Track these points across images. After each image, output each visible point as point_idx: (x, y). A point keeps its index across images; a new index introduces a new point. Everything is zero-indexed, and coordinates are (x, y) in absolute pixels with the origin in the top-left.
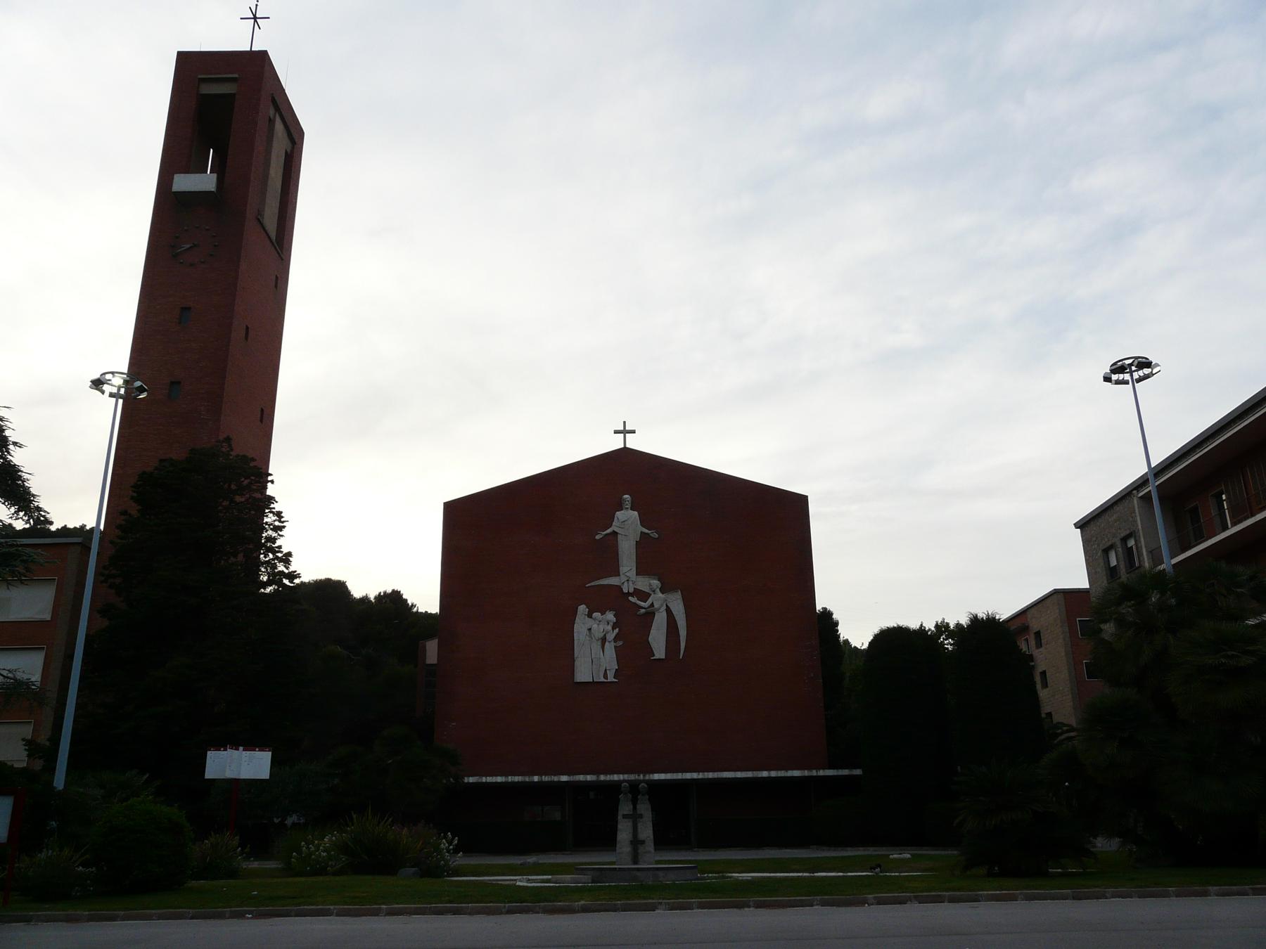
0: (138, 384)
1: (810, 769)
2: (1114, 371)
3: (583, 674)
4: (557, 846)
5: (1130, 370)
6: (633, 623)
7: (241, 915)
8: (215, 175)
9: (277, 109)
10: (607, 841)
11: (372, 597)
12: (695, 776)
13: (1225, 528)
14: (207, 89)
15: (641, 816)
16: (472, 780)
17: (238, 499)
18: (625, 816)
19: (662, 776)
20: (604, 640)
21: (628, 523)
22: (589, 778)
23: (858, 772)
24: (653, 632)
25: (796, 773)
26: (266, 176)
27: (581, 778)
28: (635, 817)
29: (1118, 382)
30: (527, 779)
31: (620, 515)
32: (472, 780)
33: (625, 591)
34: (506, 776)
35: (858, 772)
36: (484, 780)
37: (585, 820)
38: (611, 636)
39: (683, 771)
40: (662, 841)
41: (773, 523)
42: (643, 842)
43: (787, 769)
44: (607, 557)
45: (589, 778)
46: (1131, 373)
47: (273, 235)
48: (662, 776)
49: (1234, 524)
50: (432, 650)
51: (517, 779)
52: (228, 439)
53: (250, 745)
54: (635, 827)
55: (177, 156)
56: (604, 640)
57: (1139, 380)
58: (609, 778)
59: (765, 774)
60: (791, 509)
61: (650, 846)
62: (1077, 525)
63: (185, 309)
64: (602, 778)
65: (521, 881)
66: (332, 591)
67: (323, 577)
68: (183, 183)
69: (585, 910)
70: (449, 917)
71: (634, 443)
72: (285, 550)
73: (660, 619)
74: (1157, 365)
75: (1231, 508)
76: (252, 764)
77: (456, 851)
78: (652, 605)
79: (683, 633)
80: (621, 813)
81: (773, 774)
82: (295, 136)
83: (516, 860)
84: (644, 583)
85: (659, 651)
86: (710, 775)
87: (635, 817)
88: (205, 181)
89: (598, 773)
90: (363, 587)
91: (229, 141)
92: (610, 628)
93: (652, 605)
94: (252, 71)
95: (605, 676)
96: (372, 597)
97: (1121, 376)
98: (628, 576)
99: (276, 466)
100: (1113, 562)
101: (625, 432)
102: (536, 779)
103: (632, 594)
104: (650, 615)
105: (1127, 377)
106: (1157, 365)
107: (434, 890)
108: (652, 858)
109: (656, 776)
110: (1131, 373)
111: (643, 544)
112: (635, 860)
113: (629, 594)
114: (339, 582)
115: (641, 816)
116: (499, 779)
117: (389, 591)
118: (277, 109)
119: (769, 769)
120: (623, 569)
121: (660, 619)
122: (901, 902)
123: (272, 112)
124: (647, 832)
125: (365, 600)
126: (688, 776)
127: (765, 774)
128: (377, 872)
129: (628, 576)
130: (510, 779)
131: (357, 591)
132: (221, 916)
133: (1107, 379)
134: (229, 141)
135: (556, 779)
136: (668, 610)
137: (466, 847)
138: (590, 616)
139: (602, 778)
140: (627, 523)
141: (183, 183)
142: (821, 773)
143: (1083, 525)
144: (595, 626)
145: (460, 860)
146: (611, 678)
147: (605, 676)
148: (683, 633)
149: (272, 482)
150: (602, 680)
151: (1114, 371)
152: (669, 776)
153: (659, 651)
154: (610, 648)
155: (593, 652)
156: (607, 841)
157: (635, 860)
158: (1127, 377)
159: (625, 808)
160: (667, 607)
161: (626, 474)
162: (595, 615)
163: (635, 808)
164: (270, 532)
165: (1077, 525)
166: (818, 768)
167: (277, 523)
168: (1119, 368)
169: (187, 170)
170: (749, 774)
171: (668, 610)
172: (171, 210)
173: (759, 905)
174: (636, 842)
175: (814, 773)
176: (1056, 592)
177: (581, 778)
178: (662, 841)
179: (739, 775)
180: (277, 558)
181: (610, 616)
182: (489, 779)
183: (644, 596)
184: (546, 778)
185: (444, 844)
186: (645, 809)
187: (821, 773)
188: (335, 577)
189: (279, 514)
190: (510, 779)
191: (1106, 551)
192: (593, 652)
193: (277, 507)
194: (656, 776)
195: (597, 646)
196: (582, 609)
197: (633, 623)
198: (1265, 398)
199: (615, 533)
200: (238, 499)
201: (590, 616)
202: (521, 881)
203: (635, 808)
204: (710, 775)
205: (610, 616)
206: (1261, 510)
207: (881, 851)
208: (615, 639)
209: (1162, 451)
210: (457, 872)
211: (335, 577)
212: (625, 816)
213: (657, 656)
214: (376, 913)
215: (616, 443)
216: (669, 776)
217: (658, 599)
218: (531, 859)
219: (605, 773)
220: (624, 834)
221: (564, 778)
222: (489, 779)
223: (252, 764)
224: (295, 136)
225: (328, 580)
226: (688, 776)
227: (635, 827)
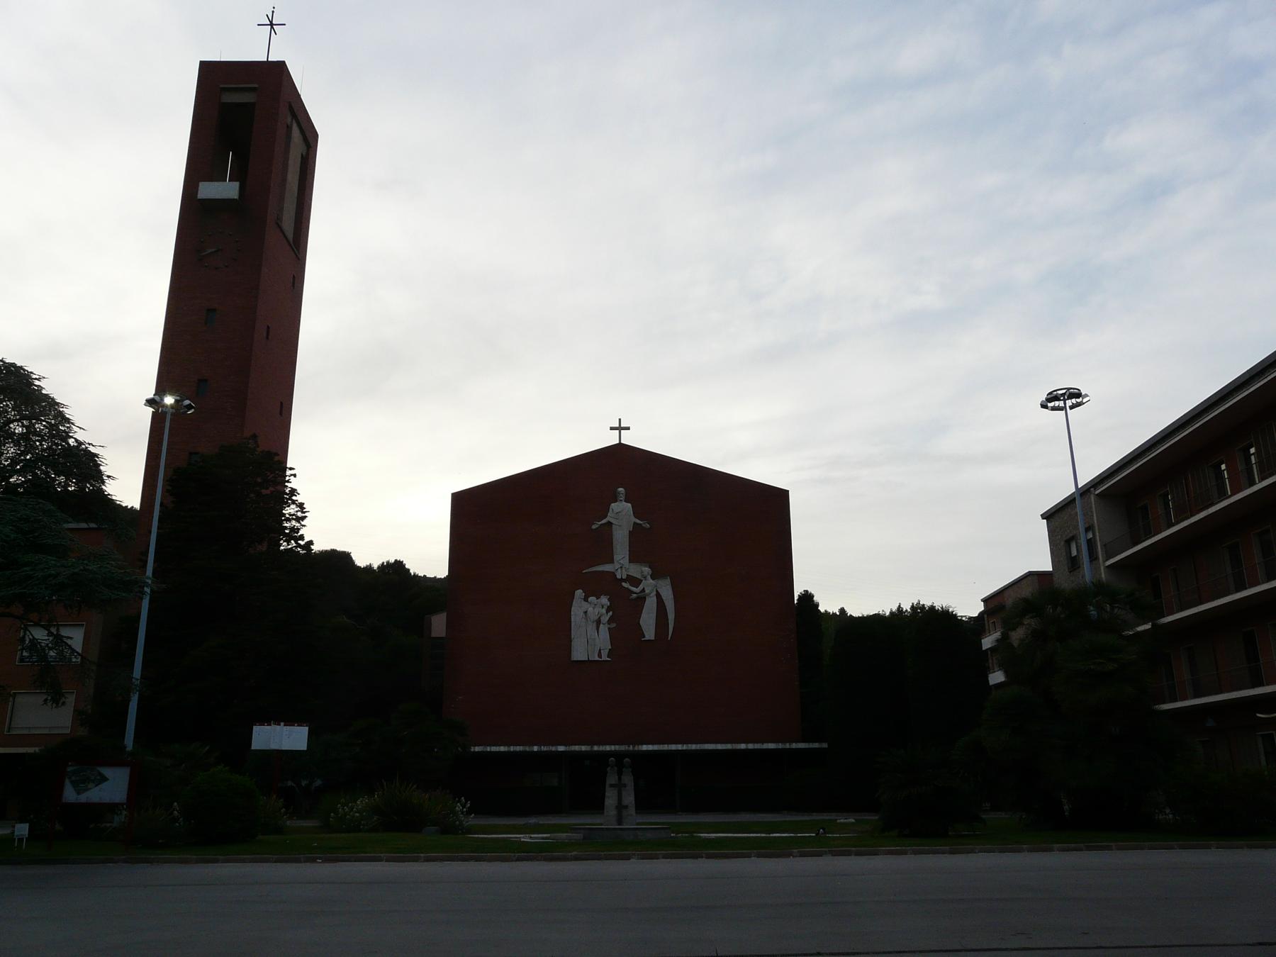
0: (187, 402)
1: (783, 742)
2: (1049, 400)
3: (579, 652)
4: (556, 810)
5: (1064, 399)
6: (625, 607)
7: (313, 860)
8: (237, 184)
9: (294, 116)
10: (596, 805)
11: (375, 567)
12: (679, 747)
13: (1252, 483)
14: (229, 98)
15: (625, 786)
16: (477, 749)
17: (264, 492)
18: (612, 786)
19: (650, 747)
20: (598, 622)
21: (621, 513)
22: (584, 748)
23: (825, 745)
24: (644, 615)
25: (771, 746)
26: (284, 180)
27: (576, 748)
28: (620, 786)
29: (1054, 409)
30: (527, 749)
31: (614, 506)
32: (477, 749)
33: (619, 577)
34: (509, 746)
35: (825, 745)
36: (489, 749)
37: (579, 786)
38: (605, 619)
39: (668, 743)
40: (644, 804)
41: (758, 514)
42: (626, 807)
43: (763, 743)
44: (602, 545)
45: (584, 748)
46: (1065, 400)
47: (290, 236)
48: (650, 747)
49: (1262, 479)
50: (438, 625)
51: (519, 748)
52: (254, 436)
53: (290, 722)
54: (619, 795)
55: (200, 165)
56: (598, 622)
57: (1071, 408)
58: (602, 748)
59: (743, 746)
60: (769, 507)
61: (632, 810)
62: (1044, 516)
63: (211, 311)
64: (596, 748)
65: (525, 838)
66: (339, 560)
67: (328, 548)
68: (209, 190)
69: (576, 859)
70: (472, 863)
71: (629, 439)
72: (307, 539)
73: (651, 603)
74: (1086, 396)
75: (1259, 463)
76: (293, 738)
77: (469, 813)
78: (643, 590)
79: (671, 616)
80: (608, 783)
81: (751, 746)
82: (310, 138)
83: (521, 821)
84: (636, 570)
85: (650, 634)
86: (694, 747)
87: (620, 786)
88: (227, 189)
89: (592, 744)
90: (367, 556)
91: (250, 143)
92: (604, 611)
93: (643, 590)
94: (270, 82)
95: (600, 655)
96: (375, 567)
97: (1057, 403)
98: (621, 563)
99: (296, 457)
100: (1074, 553)
101: (620, 428)
102: (536, 748)
103: (625, 581)
104: (642, 599)
105: (1061, 404)
106: (1086, 396)
107: (452, 841)
108: (634, 820)
109: (645, 748)
110: (1065, 400)
111: (636, 534)
112: (620, 822)
113: (622, 580)
114: (344, 553)
115: (625, 786)
116: (502, 749)
117: (392, 561)
118: (294, 116)
119: (747, 742)
120: (617, 557)
121: (651, 603)
122: (819, 855)
123: (289, 119)
124: (629, 799)
125: (369, 569)
126: (673, 747)
127: (743, 746)
128: (403, 828)
129: (621, 563)
130: (512, 749)
131: (361, 561)
132: (297, 861)
133: (1044, 406)
134: (250, 143)
135: (553, 749)
136: (658, 595)
137: (477, 809)
138: (586, 599)
139: (596, 748)
140: (621, 513)
141: (209, 190)
142: (794, 746)
143: (1048, 516)
144: (590, 609)
145: (472, 821)
146: (605, 657)
147: (600, 655)
148: (671, 616)
149: (295, 475)
150: (597, 658)
151: (1049, 400)
152: (656, 747)
153: (650, 634)
154: (604, 629)
155: (589, 632)
156: (596, 805)
157: (620, 822)
158: (1061, 404)
159: (612, 779)
160: (658, 591)
161: (620, 468)
162: (591, 599)
163: (620, 779)
164: (294, 523)
165: (1044, 516)
166: (791, 742)
167: (299, 514)
168: (1053, 397)
169: (211, 179)
170: (729, 746)
171: (658, 595)
172: (195, 214)
173: (709, 857)
174: (620, 807)
175: (787, 746)
176: (1030, 574)
177: (576, 748)
178: (644, 804)
179: (720, 747)
180: (299, 546)
181: (604, 600)
182: (494, 749)
183: (635, 581)
184: (544, 748)
185: (459, 807)
186: (628, 779)
187: (794, 746)
188: (340, 548)
189: (301, 506)
190: (512, 749)
191: (1068, 542)
192: (589, 632)
193: (299, 499)
194: (645, 748)
195: (591, 628)
196: (579, 593)
197: (625, 607)
198: (1275, 362)
199: (610, 524)
200: (264, 492)
201: (586, 599)
202: (525, 838)
203: (620, 779)
204: (694, 747)
205: (604, 600)
206: (1271, 475)
207: (832, 816)
208: (609, 622)
209: (1093, 465)
210: (469, 831)
211: (340, 548)
212: (612, 786)
213: (647, 638)
214: (416, 860)
215: (611, 439)
216: (656, 747)
217: (649, 584)
218: (533, 820)
219: (599, 744)
220: (610, 800)
221: (561, 748)
222: (494, 749)
223: (293, 738)
224: (310, 140)
225: (333, 551)
226: (673, 747)
227: (619, 795)
